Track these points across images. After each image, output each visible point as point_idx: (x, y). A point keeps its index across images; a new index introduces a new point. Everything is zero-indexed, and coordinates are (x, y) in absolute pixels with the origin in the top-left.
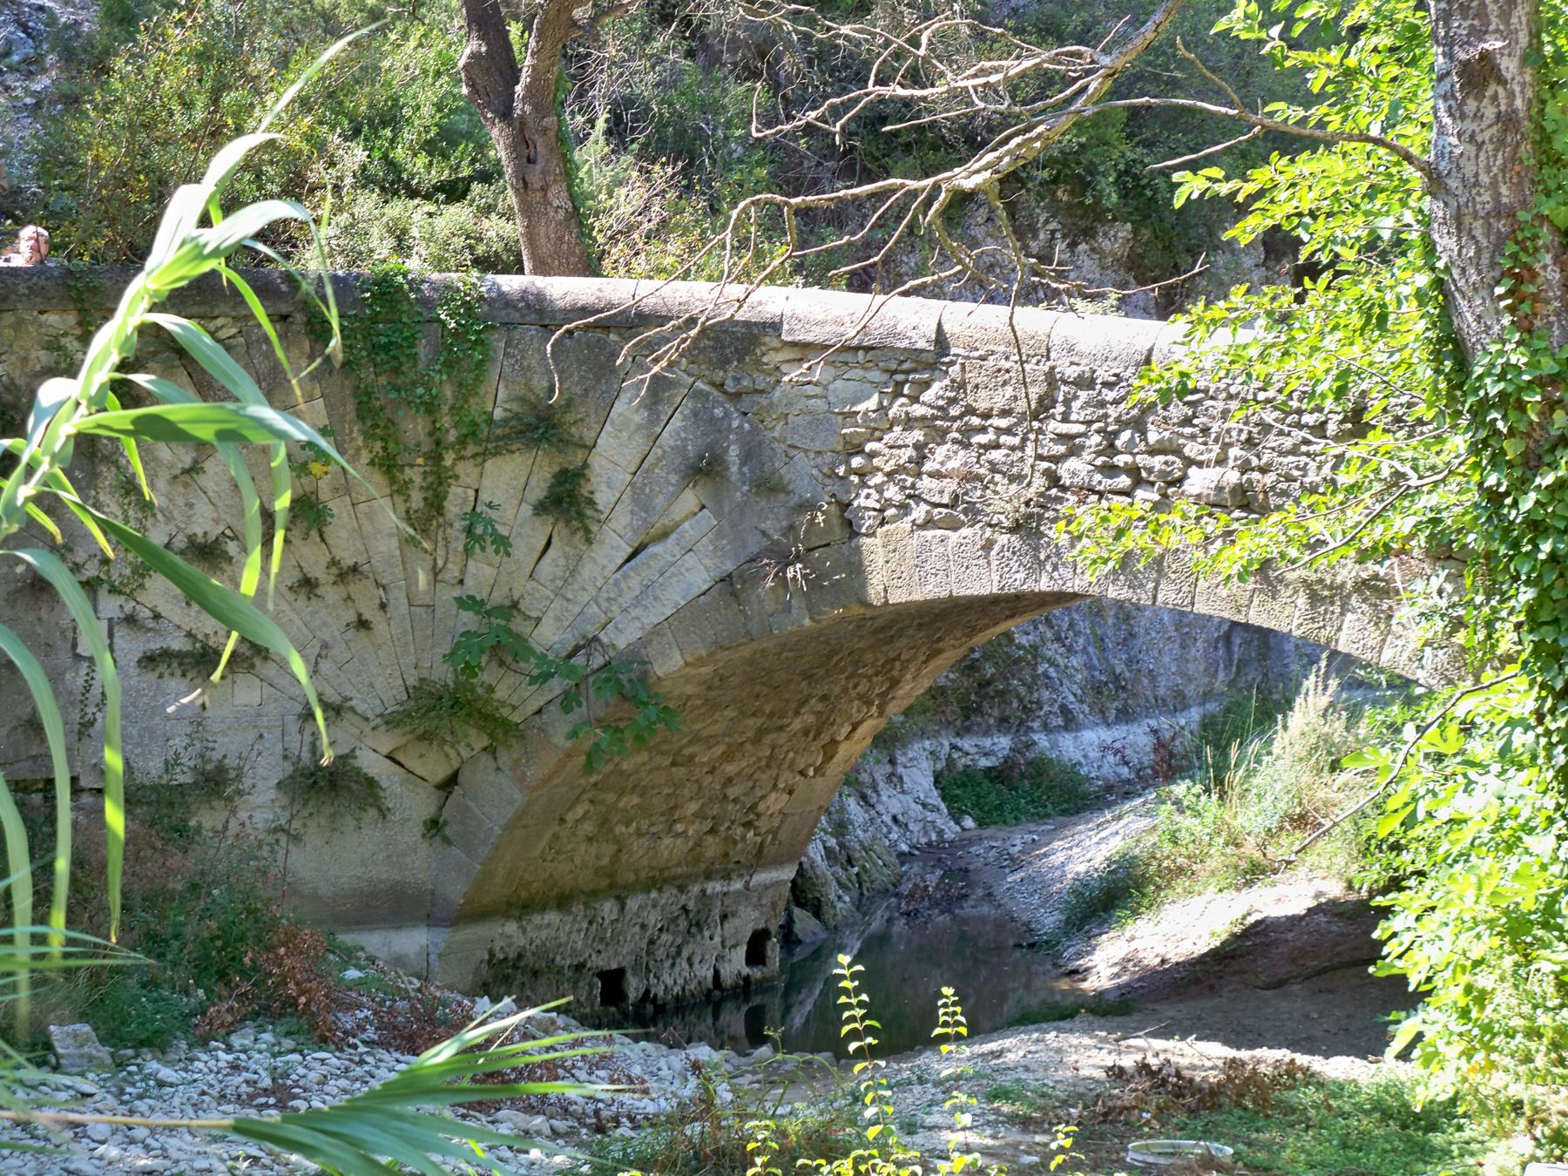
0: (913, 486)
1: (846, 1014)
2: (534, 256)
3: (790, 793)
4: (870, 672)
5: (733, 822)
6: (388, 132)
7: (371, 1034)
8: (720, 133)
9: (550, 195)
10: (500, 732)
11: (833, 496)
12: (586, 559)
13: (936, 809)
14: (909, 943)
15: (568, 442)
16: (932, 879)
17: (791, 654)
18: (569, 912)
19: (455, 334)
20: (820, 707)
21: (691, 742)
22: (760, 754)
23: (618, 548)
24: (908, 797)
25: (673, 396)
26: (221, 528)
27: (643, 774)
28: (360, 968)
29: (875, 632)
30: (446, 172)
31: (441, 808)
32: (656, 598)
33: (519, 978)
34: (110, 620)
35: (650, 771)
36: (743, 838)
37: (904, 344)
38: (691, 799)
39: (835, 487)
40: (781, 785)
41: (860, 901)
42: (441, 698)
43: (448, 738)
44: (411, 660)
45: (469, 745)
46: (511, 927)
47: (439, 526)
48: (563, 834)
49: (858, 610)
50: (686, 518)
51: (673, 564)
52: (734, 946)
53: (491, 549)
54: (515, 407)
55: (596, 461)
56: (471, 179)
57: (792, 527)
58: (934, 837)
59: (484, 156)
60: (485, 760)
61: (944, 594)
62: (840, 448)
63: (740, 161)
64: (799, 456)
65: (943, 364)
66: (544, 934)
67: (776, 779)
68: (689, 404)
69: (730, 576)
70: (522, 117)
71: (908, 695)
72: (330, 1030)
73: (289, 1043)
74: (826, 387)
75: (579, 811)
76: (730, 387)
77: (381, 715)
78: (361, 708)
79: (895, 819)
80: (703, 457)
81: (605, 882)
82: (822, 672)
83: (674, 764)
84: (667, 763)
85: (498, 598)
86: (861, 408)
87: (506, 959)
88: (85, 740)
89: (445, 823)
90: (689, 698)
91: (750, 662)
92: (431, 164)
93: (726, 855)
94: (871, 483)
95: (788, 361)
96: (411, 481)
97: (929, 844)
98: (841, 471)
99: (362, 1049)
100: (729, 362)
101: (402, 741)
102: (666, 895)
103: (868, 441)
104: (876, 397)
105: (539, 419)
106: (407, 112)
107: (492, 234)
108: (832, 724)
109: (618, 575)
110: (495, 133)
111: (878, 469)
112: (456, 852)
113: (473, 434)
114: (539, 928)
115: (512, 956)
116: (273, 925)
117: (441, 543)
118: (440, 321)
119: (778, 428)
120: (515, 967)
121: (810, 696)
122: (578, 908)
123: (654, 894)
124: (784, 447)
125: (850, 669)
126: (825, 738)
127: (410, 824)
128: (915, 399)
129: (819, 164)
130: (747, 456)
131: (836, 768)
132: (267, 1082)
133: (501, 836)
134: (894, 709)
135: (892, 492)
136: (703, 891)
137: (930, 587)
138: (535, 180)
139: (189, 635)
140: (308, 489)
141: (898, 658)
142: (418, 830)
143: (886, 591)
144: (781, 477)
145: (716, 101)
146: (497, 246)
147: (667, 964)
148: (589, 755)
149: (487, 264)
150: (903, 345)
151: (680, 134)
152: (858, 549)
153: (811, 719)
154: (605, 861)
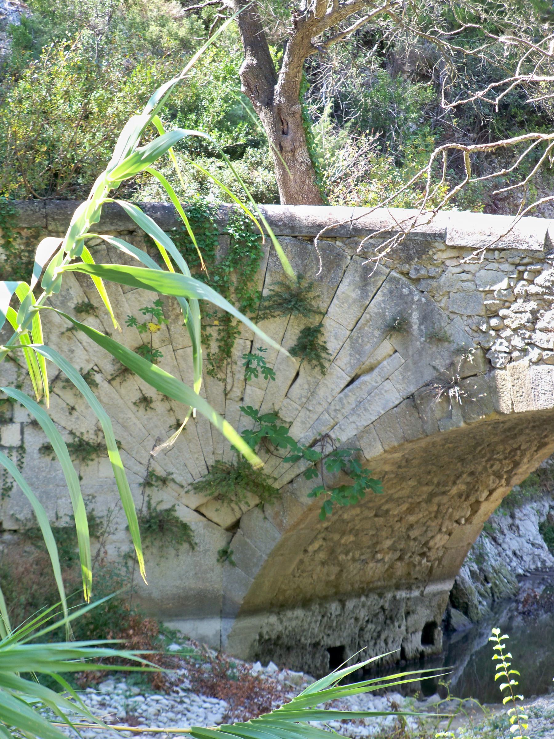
0: (530, 337)
1: (498, 666)
2: (286, 194)
3: (450, 534)
4: (501, 457)
5: (413, 553)
6: (193, 116)
7: (187, 684)
8: (402, 116)
9: (297, 154)
10: (266, 494)
11: (479, 344)
12: (321, 385)
13: (541, 547)
14: (523, 632)
15: (310, 311)
16: (539, 591)
17: (451, 445)
18: (310, 610)
19: (239, 242)
20: (469, 479)
21: (387, 502)
22: (431, 509)
23: (341, 378)
24: (523, 540)
25: (376, 281)
26: (91, 365)
27: (357, 522)
28: (180, 644)
29: (505, 431)
30: (230, 141)
31: (229, 543)
32: (365, 409)
33: (278, 651)
34: (22, 423)
35: (361, 520)
36: (420, 563)
37: (524, 247)
38: (387, 538)
39: (480, 338)
40: (444, 530)
41: (493, 605)
42: (229, 473)
43: (234, 498)
44: (210, 449)
45: (247, 503)
46: (273, 619)
47: (228, 364)
48: (307, 560)
49: (494, 417)
50: (385, 358)
51: (377, 388)
52: (414, 632)
53: (262, 376)
54: (277, 288)
55: (328, 323)
56: (246, 145)
57: (452, 364)
58: (539, 565)
59: (255, 131)
60: (257, 513)
61: (536, 410)
62: (483, 313)
63: (415, 134)
64: (457, 319)
65: (550, 259)
66: (294, 623)
67: (441, 526)
68: (387, 286)
69: (413, 395)
70: (279, 105)
71: (525, 472)
72: (161, 682)
73: (136, 690)
74: (474, 275)
75: (316, 545)
76: (413, 275)
77: (191, 484)
78: (179, 479)
79: (515, 553)
80: (396, 320)
81: (332, 591)
82: (470, 457)
83: (376, 515)
84: (372, 514)
85: (265, 409)
86: (496, 287)
87: (270, 639)
88: (7, 499)
89: (232, 552)
90: (386, 473)
91: (425, 450)
92: (220, 136)
93: (409, 574)
94: (503, 335)
95: (450, 258)
96: (211, 335)
97: (537, 569)
98: (484, 327)
99: (182, 694)
100: (411, 259)
101: (204, 500)
102: (371, 599)
103: (501, 308)
104: (506, 280)
105: (292, 296)
106: (205, 103)
107: (259, 180)
108: (477, 491)
109: (341, 395)
110: (262, 115)
111: (508, 327)
112: (239, 571)
113: (250, 305)
114: (290, 620)
115: (274, 636)
116: (125, 617)
117: (229, 375)
118: (228, 234)
119: (444, 301)
120: (276, 644)
121: (463, 473)
122: (315, 607)
123: (363, 599)
124: (447, 313)
125: (488, 455)
126: (472, 499)
127: (209, 553)
128: (531, 282)
129: (465, 135)
130: (425, 318)
131: (479, 519)
132: (123, 714)
133: (267, 561)
134: (516, 480)
135: (517, 342)
136: (394, 597)
137: (541, 402)
138: (287, 145)
139: (71, 433)
140: (146, 341)
141: (519, 448)
142: (211, 559)
143: (512, 404)
144: (445, 332)
145: (399, 95)
146: (263, 188)
147: (372, 643)
148: (323, 509)
149: (259, 198)
150: (523, 248)
151: (377, 117)
152: (494, 378)
153: (463, 487)
154: (333, 577)
